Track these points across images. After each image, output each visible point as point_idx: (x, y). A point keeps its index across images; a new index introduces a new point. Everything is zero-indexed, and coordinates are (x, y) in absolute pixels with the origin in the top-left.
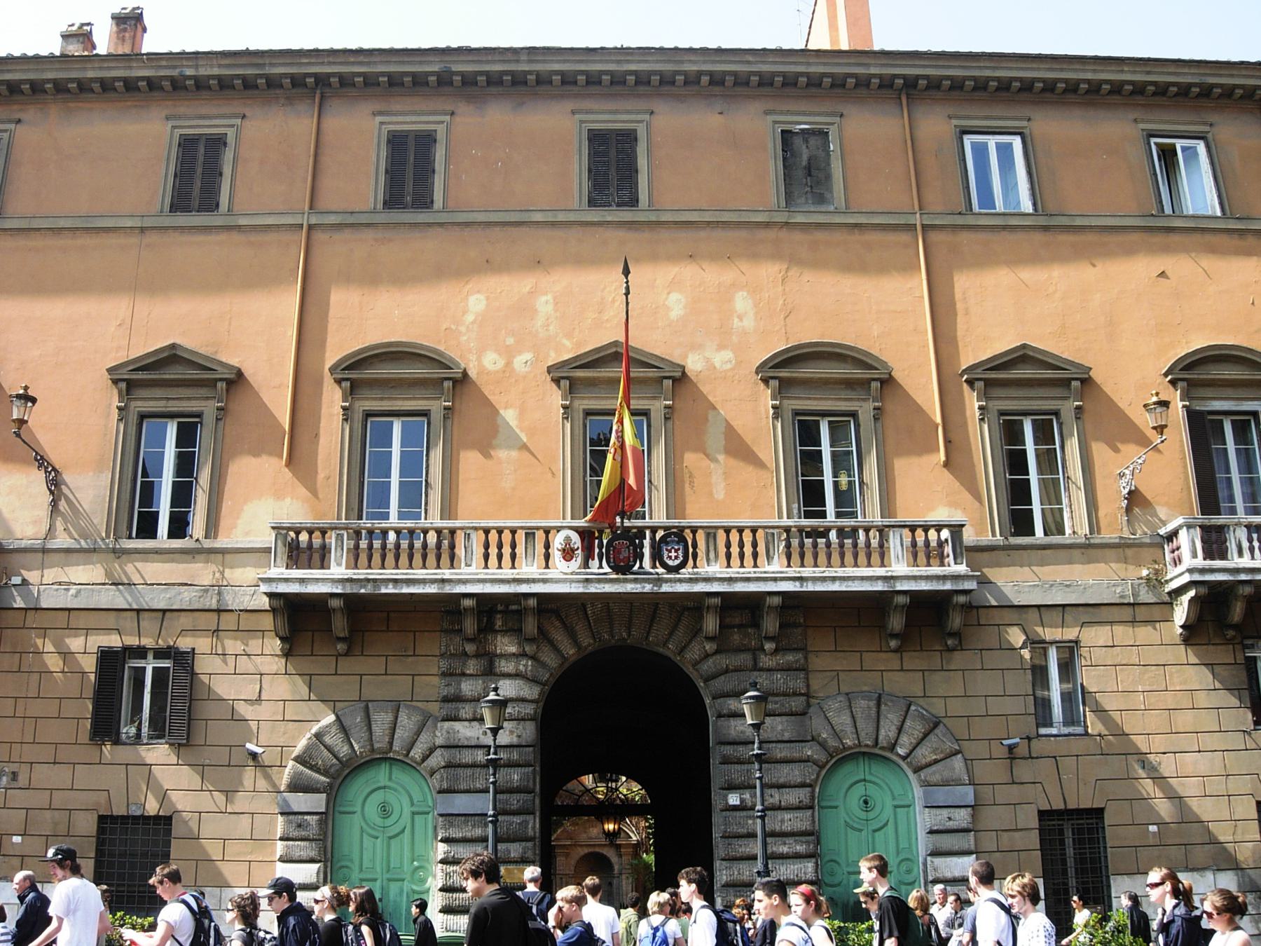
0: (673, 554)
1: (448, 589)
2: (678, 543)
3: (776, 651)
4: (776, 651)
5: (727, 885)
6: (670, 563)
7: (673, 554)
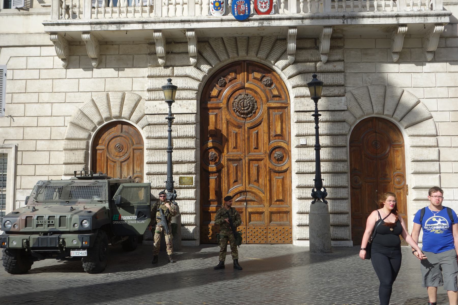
1: (147, 27)
3: (328, 62)
4: (328, 62)
5: (298, 187)
6: (262, 10)
7: (264, 5)
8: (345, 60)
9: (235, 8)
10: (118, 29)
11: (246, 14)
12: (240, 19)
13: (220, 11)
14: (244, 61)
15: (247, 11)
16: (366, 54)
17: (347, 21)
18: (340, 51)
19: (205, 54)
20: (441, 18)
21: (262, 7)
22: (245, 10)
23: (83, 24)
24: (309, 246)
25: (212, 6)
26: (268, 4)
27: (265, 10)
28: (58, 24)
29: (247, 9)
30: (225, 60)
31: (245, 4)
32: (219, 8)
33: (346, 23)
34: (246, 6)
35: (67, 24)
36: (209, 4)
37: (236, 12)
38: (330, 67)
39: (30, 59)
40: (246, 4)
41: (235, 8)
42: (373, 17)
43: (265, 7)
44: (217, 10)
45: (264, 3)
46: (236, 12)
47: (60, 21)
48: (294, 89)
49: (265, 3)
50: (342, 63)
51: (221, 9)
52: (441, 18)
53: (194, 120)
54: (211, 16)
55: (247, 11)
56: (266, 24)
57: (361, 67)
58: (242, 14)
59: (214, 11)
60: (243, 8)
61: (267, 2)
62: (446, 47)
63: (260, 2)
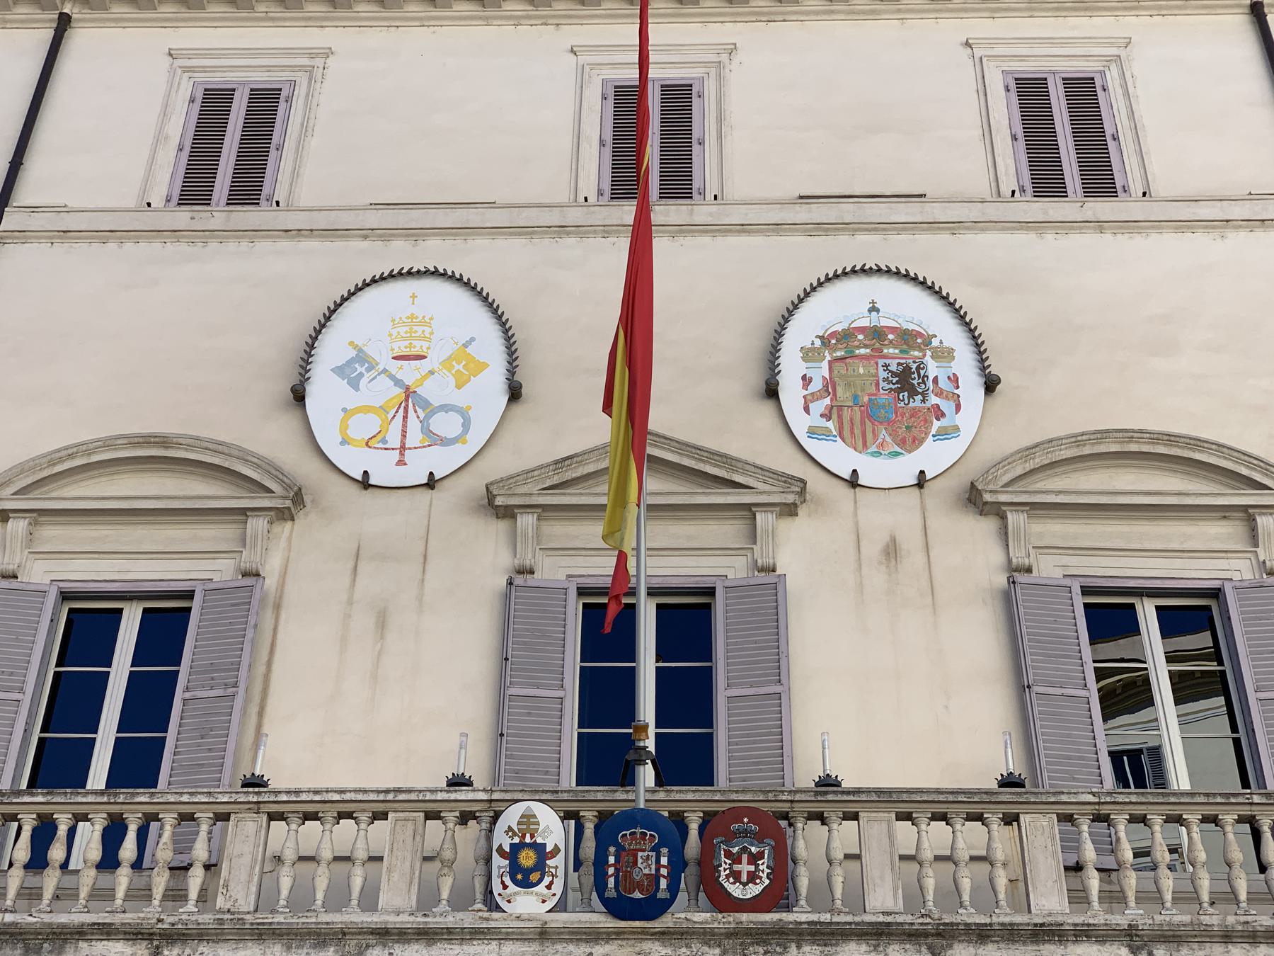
0: (745, 868)
2: (759, 838)
6: (736, 890)
7: (745, 868)
9: (612, 860)
11: (660, 895)
13: (541, 888)
15: (663, 883)
21: (736, 876)
22: (657, 877)
24: (654, 241)
25: (499, 863)
26: (763, 866)
27: (754, 890)
29: (664, 871)
31: (656, 849)
32: (534, 877)
34: (664, 861)
36: (488, 860)
40: (664, 850)
41: (612, 860)
43: (753, 878)
44: (526, 884)
45: (745, 857)
49: (754, 859)
51: (547, 880)
53: (546, 577)
54: (496, 915)
55: (663, 883)
58: (637, 895)
59: (512, 888)
60: (645, 865)
61: (760, 855)
63: (728, 855)
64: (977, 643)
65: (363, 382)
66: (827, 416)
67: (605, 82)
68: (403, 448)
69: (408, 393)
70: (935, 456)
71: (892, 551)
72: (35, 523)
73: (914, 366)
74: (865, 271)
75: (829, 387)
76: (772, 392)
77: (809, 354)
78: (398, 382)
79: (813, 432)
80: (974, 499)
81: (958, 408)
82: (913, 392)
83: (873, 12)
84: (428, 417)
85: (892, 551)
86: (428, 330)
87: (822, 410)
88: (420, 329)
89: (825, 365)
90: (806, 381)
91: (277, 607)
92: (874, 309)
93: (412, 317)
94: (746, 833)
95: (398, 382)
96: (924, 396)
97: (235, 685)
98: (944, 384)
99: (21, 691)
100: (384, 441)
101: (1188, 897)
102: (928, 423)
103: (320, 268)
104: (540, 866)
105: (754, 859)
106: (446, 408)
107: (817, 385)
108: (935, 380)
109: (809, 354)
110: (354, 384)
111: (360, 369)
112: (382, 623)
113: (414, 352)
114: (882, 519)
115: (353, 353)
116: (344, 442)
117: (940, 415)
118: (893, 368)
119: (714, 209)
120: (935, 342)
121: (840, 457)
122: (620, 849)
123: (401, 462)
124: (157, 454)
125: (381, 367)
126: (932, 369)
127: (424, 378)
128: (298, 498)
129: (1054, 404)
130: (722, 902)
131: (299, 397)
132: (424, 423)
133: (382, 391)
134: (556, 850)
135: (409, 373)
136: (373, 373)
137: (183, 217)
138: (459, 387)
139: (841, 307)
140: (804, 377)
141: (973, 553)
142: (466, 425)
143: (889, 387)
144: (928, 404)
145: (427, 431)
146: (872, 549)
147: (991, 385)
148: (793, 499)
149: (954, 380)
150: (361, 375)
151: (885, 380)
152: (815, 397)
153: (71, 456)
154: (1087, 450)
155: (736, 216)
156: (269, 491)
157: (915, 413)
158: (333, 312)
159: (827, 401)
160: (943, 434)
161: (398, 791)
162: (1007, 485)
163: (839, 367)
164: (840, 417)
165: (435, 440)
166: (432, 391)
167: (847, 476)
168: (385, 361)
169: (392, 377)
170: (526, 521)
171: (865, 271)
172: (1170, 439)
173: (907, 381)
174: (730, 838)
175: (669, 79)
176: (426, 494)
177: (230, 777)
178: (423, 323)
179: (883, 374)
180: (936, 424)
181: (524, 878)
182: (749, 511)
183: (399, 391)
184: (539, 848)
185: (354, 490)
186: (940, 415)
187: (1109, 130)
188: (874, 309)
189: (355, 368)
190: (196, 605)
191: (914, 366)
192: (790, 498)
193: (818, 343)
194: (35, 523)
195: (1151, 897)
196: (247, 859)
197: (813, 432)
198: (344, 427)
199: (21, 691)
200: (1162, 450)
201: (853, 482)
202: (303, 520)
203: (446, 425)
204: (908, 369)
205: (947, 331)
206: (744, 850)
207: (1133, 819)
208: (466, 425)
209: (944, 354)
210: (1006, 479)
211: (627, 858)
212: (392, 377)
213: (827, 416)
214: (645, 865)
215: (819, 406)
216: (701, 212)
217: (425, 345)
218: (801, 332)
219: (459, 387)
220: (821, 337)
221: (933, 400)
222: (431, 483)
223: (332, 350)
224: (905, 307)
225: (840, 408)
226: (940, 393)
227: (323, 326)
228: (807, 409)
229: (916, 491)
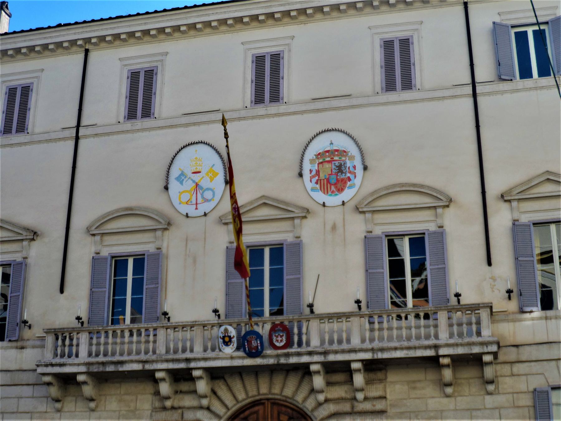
1: (148, 367)
2: (283, 331)
3: (366, 399)
4: (366, 399)
6: (278, 344)
7: (279, 339)
8: (388, 397)
10: (116, 370)
12: (252, 354)
13: (231, 346)
14: (268, 399)
15: (259, 348)
16: (414, 388)
17: (377, 354)
18: (381, 386)
19: (220, 393)
20: (487, 347)
21: (277, 341)
22: (257, 347)
23: (79, 365)
25: (221, 340)
26: (284, 338)
27: (282, 344)
28: (52, 365)
29: (259, 345)
30: (244, 400)
31: (256, 340)
32: (229, 343)
33: (376, 357)
34: (259, 342)
35: (61, 365)
37: (247, 349)
38: (367, 406)
39: (22, 401)
42: (409, 348)
43: (281, 341)
46: (247, 349)
47: (54, 361)
48: (512, 298)
49: (281, 336)
50: (384, 400)
51: (232, 344)
52: (487, 347)
54: (221, 353)
55: (259, 348)
56: (283, 361)
57: (408, 404)
58: (254, 351)
59: (224, 347)
61: (283, 336)
62: (513, 375)
63: (275, 336)
64: (356, 256)
65: (184, 181)
66: (317, 183)
67: (253, 55)
68: (197, 204)
69: (197, 185)
70: (347, 194)
71: (334, 228)
72: (102, 236)
73: (343, 163)
74: (328, 130)
75: (318, 172)
76: (301, 175)
77: (312, 162)
78: (194, 181)
79: (313, 189)
80: (358, 210)
81: (355, 177)
82: (342, 172)
83: (339, 17)
84: (203, 192)
85: (334, 228)
86: (201, 163)
87: (315, 181)
88: (198, 162)
89: (316, 165)
90: (311, 171)
91: (167, 258)
92: (332, 144)
93: (196, 158)
94: (279, 330)
95: (194, 181)
96: (345, 173)
97: (158, 283)
98: (352, 169)
99: (105, 288)
100: (191, 202)
101: (390, 339)
102: (346, 183)
103: (169, 140)
104: (230, 341)
105: (281, 336)
106: (208, 189)
107: (314, 173)
108: (349, 168)
109: (312, 162)
110: (181, 183)
111: (183, 178)
112: (195, 261)
113: (198, 170)
114: (333, 216)
115: (180, 172)
116: (180, 203)
117: (349, 179)
118: (337, 164)
119: (285, 107)
120: (349, 154)
121: (320, 197)
122: (248, 341)
123: (196, 209)
124: (130, 213)
125: (188, 177)
126: (349, 164)
127: (201, 179)
128: (169, 224)
129: (384, 174)
130: (276, 348)
131: (166, 188)
132: (202, 195)
133: (189, 185)
134: (234, 337)
135: (197, 177)
136: (186, 179)
137: (128, 125)
138: (211, 182)
139: (321, 144)
140: (310, 170)
141: (357, 227)
142: (214, 195)
143: (334, 174)
144: (346, 177)
145: (203, 197)
146: (329, 227)
147: (365, 168)
148: (306, 213)
149: (354, 167)
150: (183, 180)
151: (334, 169)
152: (313, 177)
153: (108, 216)
154: (390, 191)
155: (292, 109)
156: (161, 223)
157: (342, 180)
158: (173, 159)
159: (317, 178)
160: (351, 187)
161: (196, 322)
162: (365, 206)
163: (321, 166)
164: (321, 183)
165: (207, 201)
166: (205, 184)
167: (322, 203)
168: (190, 175)
169: (192, 180)
170: (514, 204)
171: (328, 130)
172: (414, 185)
173: (340, 169)
174: (275, 331)
175: (273, 52)
176: (204, 218)
177: (159, 314)
178: (199, 160)
179: (334, 167)
180: (349, 183)
181: (227, 344)
182: (293, 218)
183: (194, 185)
184: (230, 337)
185: (184, 218)
186: (349, 179)
187: (254, 84)
188: (332, 144)
189: (181, 178)
190: (146, 257)
191: (343, 163)
192: (304, 214)
193: (315, 157)
194: (102, 236)
195: (381, 339)
196: (162, 340)
197: (313, 189)
198: (180, 198)
199: (105, 288)
200: (412, 189)
201: (324, 205)
202: (172, 229)
203: (208, 195)
204: (341, 164)
205: (353, 150)
206: (279, 334)
207: (379, 316)
208: (214, 195)
209: (352, 158)
210: (366, 203)
211: (249, 342)
212: (192, 180)
213: (317, 183)
214: (254, 344)
215: (314, 180)
216: (282, 108)
217: (201, 167)
218: (310, 154)
219: (211, 182)
220: (315, 155)
221: (348, 175)
222: (205, 215)
223: (175, 172)
224: (341, 142)
225: (321, 180)
226: (350, 172)
227: (171, 164)
228: (311, 181)
229: (342, 206)
